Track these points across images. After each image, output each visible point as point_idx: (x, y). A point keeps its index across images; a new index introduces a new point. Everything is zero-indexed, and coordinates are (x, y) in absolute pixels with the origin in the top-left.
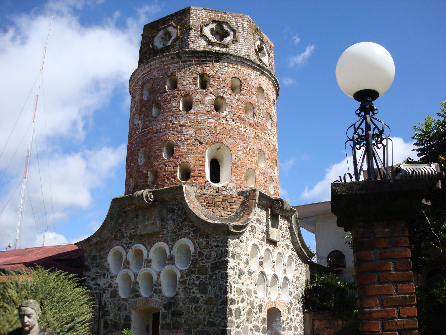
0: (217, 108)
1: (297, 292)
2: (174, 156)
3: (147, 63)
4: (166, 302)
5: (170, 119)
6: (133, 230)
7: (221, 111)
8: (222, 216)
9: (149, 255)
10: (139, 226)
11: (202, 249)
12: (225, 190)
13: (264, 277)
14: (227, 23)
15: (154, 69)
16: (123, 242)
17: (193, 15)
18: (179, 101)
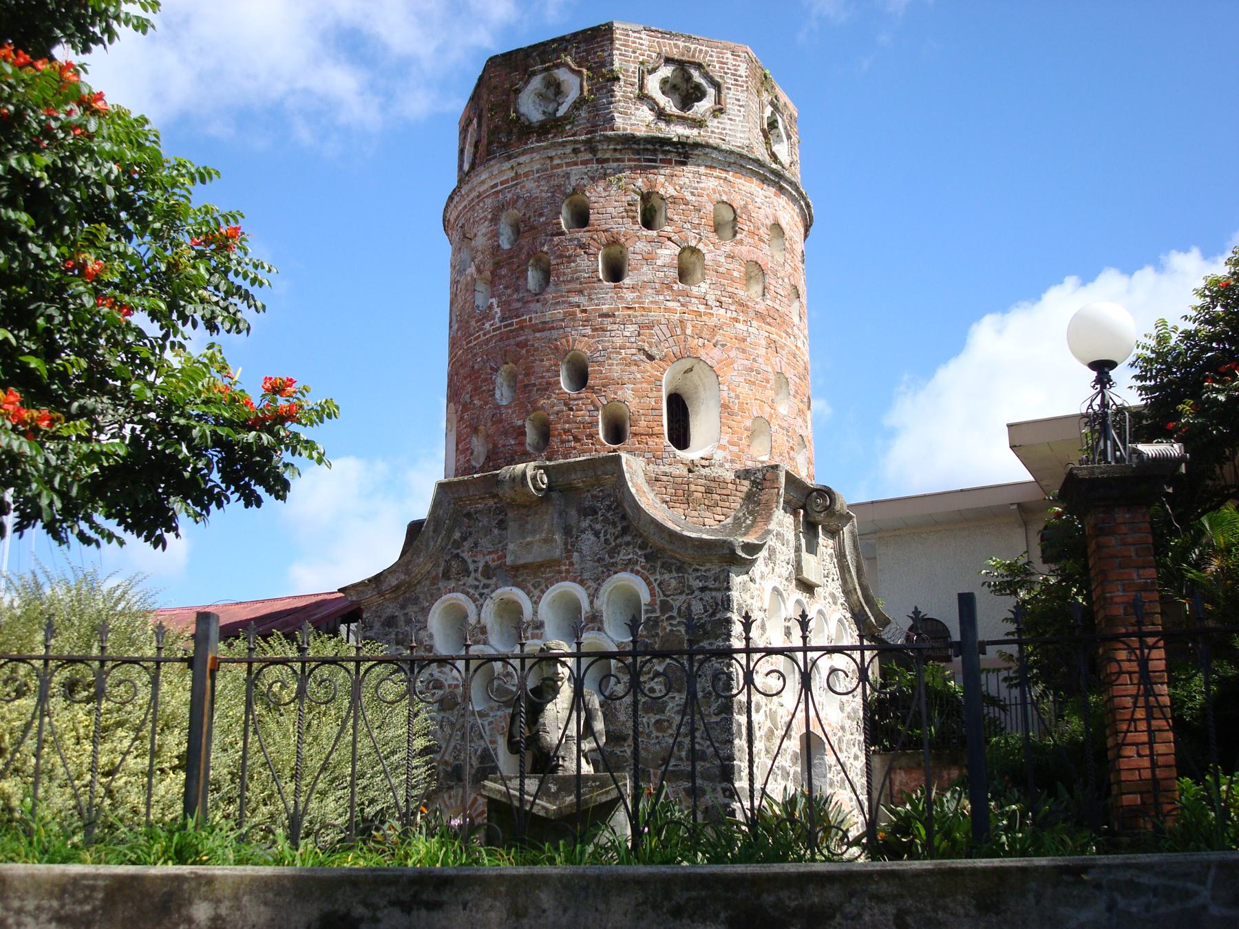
1: (854, 704)
3: (509, 158)
5: (575, 299)
6: (491, 557)
7: (690, 281)
8: (704, 525)
10: (511, 546)
11: (669, 596)
14: (699, 66)
15: (526, 175)
17: (621, 45)
18: (595, 255)
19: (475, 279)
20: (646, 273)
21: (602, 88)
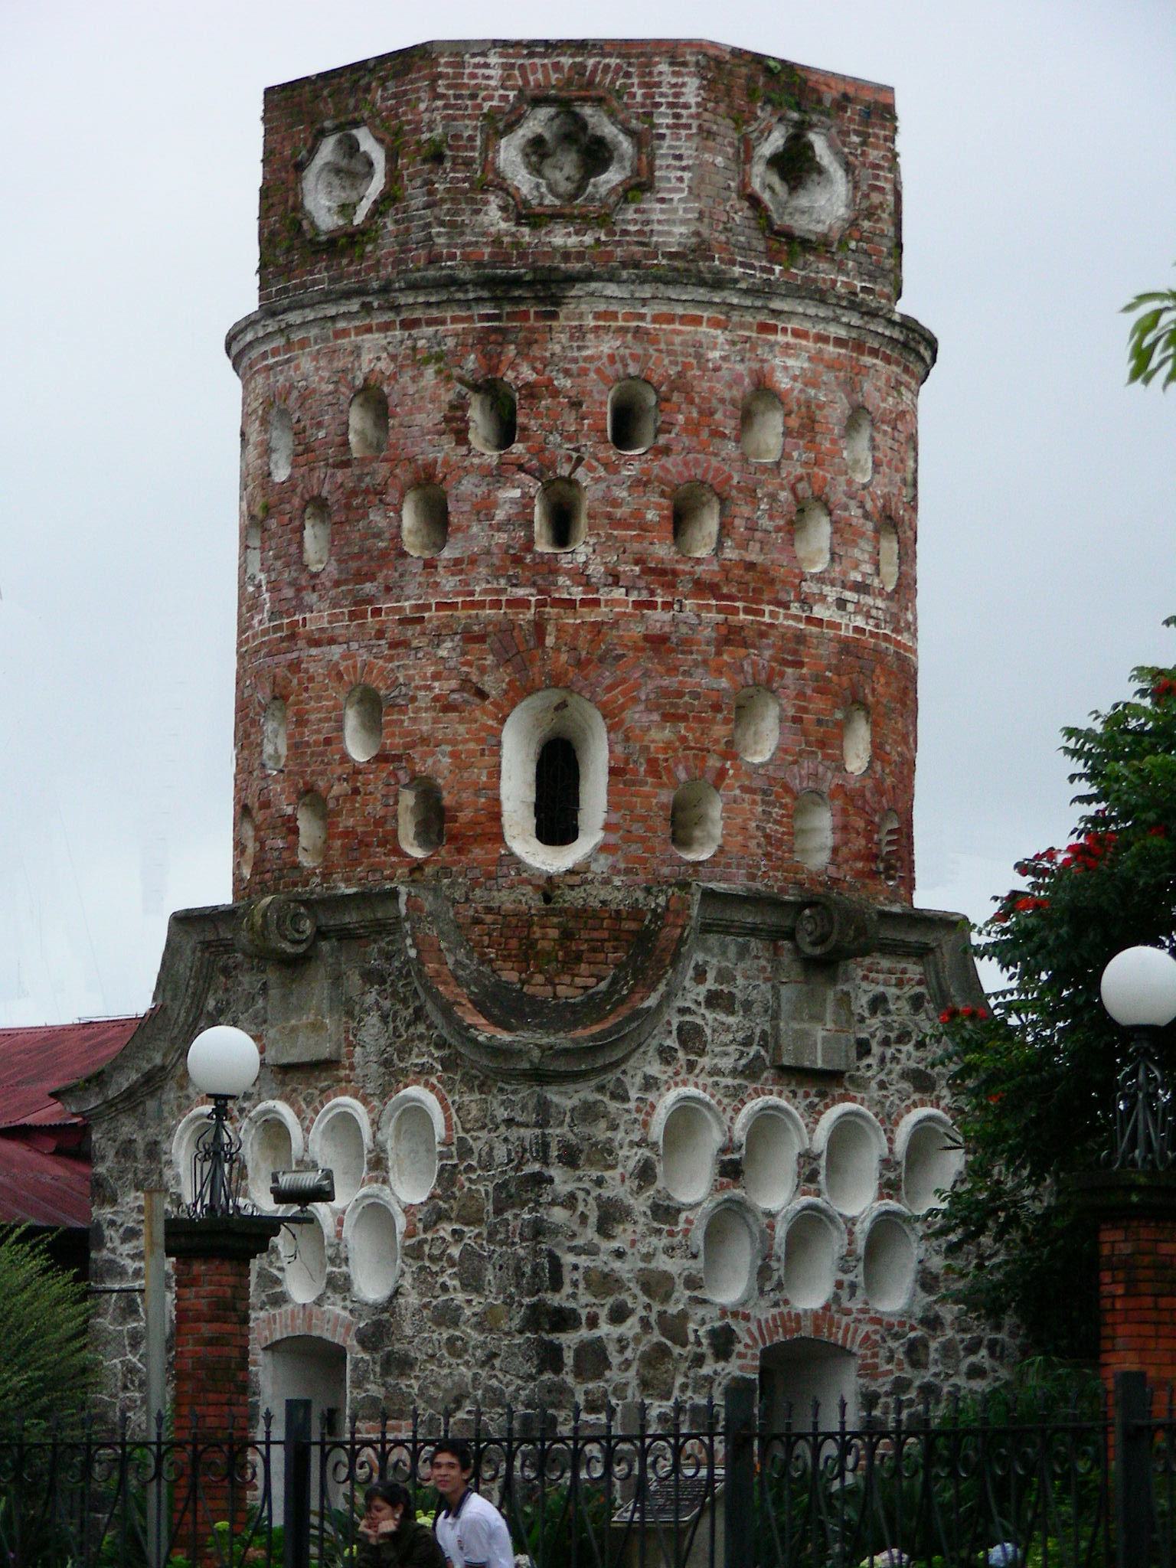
17: (448, 87)
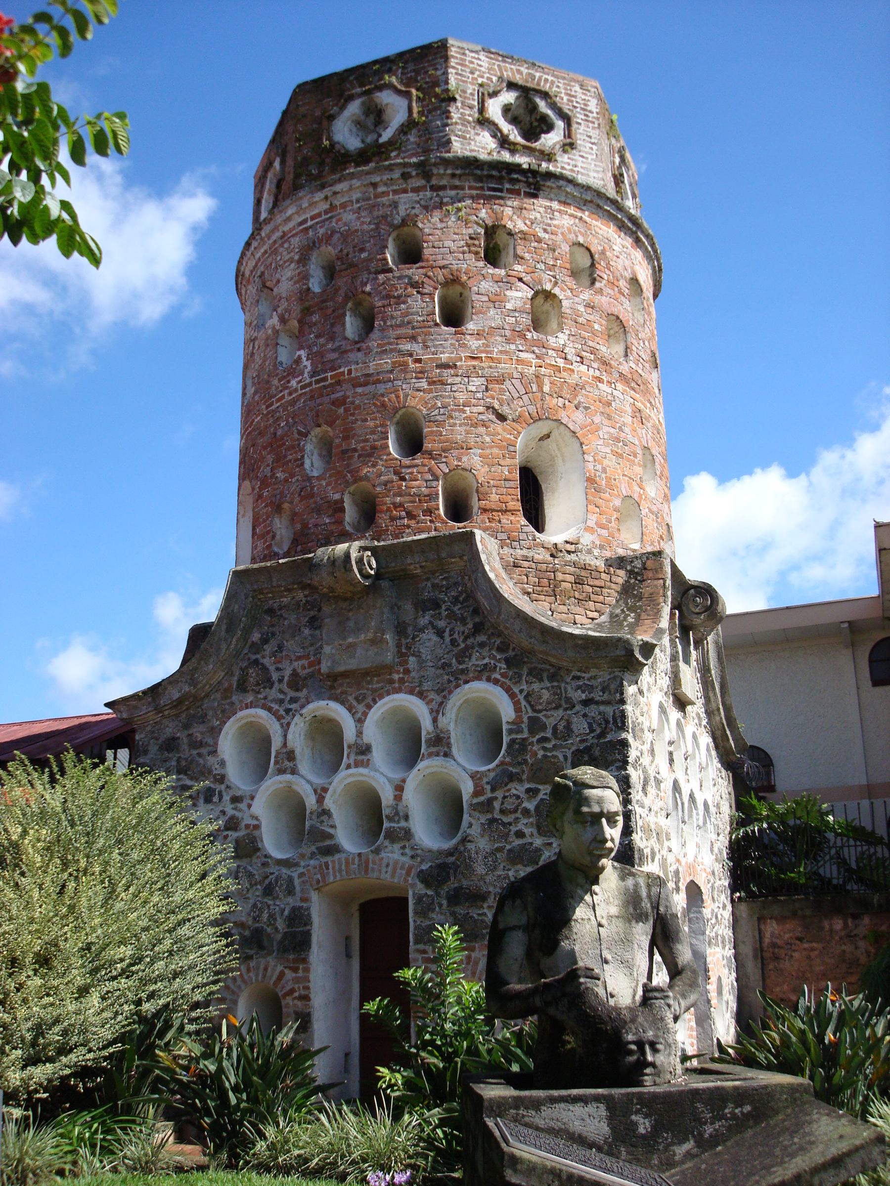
0: (537, 324)
2: (426, 451)
3: (323, 187)
4: (430, 864)
5: (407, 346)
6: (300, 663)
8: (575, 623)
9: (361, 733)
10: (327, 649)
11: (540, 711)
12: (573, 552)
13: (677, 795)
14: (545, 95)
15: (343, 206)
16: (270, 698)
17: (457, 63)
18: (431, 295)
19: (277, 332)
20: (493, 318)
21: (435, 109)
